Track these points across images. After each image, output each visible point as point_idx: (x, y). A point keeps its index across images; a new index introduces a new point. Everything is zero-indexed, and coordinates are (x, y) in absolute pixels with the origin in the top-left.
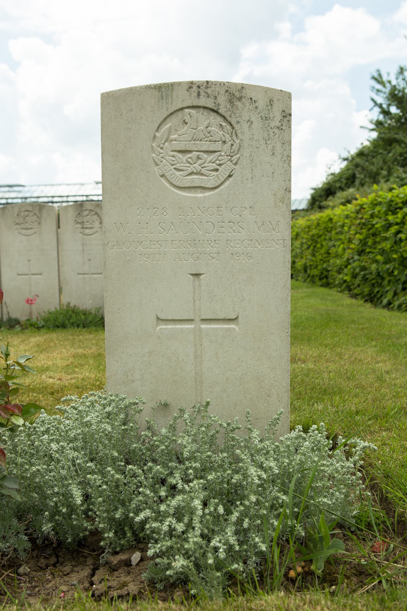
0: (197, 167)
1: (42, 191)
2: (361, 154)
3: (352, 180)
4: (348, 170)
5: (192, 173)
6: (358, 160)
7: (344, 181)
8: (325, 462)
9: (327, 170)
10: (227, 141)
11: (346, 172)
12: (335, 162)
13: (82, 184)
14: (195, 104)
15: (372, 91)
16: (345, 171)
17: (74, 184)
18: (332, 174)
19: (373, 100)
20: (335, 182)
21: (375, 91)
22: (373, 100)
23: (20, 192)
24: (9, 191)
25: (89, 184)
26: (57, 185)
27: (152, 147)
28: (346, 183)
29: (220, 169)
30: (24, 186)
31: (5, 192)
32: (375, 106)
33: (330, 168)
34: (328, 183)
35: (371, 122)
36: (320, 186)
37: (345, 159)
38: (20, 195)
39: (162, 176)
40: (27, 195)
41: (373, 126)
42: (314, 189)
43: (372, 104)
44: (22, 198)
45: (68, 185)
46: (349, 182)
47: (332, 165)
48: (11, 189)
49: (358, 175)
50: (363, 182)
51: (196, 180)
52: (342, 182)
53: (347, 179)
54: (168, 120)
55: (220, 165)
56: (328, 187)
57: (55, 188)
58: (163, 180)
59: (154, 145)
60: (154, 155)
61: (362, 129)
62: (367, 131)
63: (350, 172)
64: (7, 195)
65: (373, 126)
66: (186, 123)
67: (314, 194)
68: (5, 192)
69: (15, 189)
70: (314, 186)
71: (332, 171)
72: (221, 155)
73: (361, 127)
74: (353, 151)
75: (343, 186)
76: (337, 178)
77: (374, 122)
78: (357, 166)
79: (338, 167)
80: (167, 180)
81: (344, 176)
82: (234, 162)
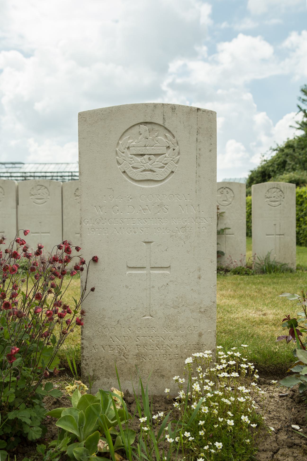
0: (148, 166)
1: (37, 168)
2: (289, 146)
3: (282, 165)
4: (279, 158)
5: (144, 170)
6: (286, 151)
7: (276, 166)
8: (40, 315)
9: (262, 157)
10: (171, 146)
11: (277, 159)
12: (267, 151)
13: (68, 164)
14: (148, 121)
15: (299, 100)
16: (276, 159)
17: (62, 164)
18: (265, 161)
19: (299, 107)
20: (268, 166)
21: (301, 100)
22: (299, 107)
23: (21, 168)
24: (12, 168)
25: (73, 163)
26: (48, 164)
27: (116, 151)
28: (278, 168)
29: (166, 166)
30: (24, 164)
31: (10, 168)
32: (300, 111)
33: (263, 156)
34: (263, 167)
35: (297, 123)
36: (257, 169)
37: (274, 150)
38: (22, 170)
39: (124, 172)
40: (26, 171)
41: (298, 126)
42: (252, 171)
43: (298, 110)
44: (23, 173)
45: (57, 164)
46: (280, 167)
47: (265, 153)
48: (14, 166)
49: (289, 162)
50: (294, 167)
51: (149, 175)
52: (274, 167)
53: (278, 165)
54: (125, 134)
55: (166, 164)
56: (263, 170)
57: (47, 166)
58: (124, 176)
59: (117, 149)
60: (117, 157)
61: (291, 128)
62: (295, 129)
63: (281, 159)
64: (10, 170)
65: (298, 126)
66: (141, 134)
67: (251, 175)
68: (10, 168)
69: (17, 165)
70: (252, 169)
71: (265, 158)
72: (165, 157)
73: (290, 126)
74: (282, 144)
75: (275, 170)
76: (270, 164)
77: (300, 122)
78: (287, 155)
79: (271, 155)
80: (127, 175)
81: (276, 163)
82: (176, 161)
